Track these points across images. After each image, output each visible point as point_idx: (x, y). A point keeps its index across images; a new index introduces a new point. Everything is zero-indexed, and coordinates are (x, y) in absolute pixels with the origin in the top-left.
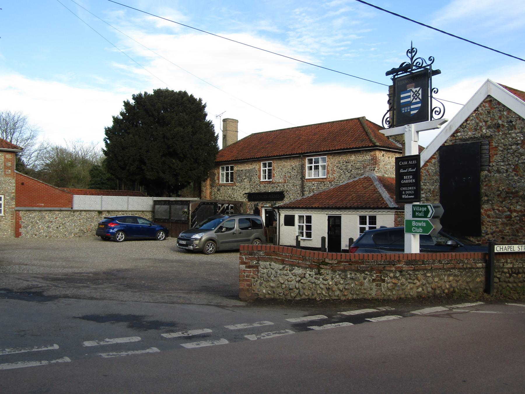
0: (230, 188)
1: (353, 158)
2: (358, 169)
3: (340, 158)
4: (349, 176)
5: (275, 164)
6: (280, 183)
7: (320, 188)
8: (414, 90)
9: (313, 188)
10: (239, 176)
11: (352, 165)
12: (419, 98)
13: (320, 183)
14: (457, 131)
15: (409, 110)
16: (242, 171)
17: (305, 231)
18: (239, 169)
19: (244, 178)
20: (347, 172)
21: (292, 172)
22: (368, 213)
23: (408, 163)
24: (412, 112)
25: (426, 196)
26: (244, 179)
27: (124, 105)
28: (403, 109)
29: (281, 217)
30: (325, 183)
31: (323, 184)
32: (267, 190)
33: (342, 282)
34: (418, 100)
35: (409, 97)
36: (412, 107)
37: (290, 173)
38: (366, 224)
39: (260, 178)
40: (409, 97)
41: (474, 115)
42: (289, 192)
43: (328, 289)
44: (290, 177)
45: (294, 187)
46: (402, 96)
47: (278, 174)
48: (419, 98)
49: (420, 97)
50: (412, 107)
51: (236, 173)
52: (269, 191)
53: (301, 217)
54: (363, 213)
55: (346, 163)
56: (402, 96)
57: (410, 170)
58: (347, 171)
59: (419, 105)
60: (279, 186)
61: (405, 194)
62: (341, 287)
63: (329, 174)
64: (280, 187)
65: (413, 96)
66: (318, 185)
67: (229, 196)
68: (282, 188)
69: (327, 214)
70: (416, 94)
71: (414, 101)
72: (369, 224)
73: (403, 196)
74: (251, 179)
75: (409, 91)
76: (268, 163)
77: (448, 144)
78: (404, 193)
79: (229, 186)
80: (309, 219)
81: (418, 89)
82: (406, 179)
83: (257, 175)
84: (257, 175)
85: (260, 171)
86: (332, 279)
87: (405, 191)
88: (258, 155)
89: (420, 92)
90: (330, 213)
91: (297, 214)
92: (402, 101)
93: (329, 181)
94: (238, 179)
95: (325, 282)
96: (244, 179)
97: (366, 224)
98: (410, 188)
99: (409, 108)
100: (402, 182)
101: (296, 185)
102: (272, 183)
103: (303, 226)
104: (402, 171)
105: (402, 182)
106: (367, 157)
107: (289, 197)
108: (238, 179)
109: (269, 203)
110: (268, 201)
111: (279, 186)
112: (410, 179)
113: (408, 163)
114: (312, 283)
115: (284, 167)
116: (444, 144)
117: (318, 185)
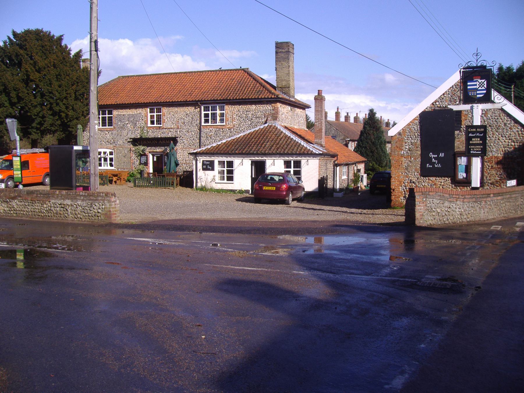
0: (109, 133)
1: (254, 107)
2: (259, 117)
3: (240, 106)
4: (250, 124)
5: (165, 110)
6: (172, 128)
7: (218, 134)
8: (480, 81)
9: (210, 134)
10: (120, 120)
11: (252, 114)
12: (484, 87)
13: (218, 129)
14: (435, 102)
15: (475, 94)
16: (123, 115)
17: (226, 175)
18: (119, 113)
19: (127, 122)
20: (247, 120)
21: (186, 119)
22: (292, 159)
23: (476, 130)
24: (478, 96)
25: (409, 148)
26: (127, 124)
27: (248, 69)
28: (470, 93)
29: (198, 162)
30: (224, 129)
31: (222, 131)
32: (157, 135)
33: (467, 209)
34: (483, 88)
35: (476, 85)
36: (478, 92)
37: (184, 119)
38: (291, 168)
39: (147, 124)
40: (476, 85)
41: (450, 90)
42: (183, 138)
43: (461, 214)
44: (184, 123)
45: (189, 133)
46: (468, 84)
47: (169, 120)
48: (484, 87)
49: (485, 86)
50: (478, 92)
51: (116, 118)
52: (159, 137)
53: (220, 162)
54: (287, 159)
55: (247, 111)
56: (468, 84)
57: (478, 134)
58: (248, 119)
59: (485, 92)
60: (170, 132)
61: (473, 150)
62: (467, 212)
63: (228, 121)
64: (172, 133)
65: (479, 85)
66: (216, 131)
67: (107, 141)
68: (174, 134)
69: (250, 159)
70: (481, 85)
71: (480, 88)
72: (294, 168)
73: (472, 152)
74: (136, 124)
75: (476, 81)
76: (204, 111)
77: (428, 110)
78: (472, 149)
79: (107, 131)
80: (230, 164)
81: (483, 81)
82: (474, 141)
83: (143, 120)
84: (143, 120)
85: (147, 116)
86: (463, 208)
87: (473, 148)
88: (142, 100)
89: (485, 83)
90: (254, 158)
91: (216, 160)
92: (469, 87)
93: (228, 128)
94: (119, 123)
95: (460, 210)
96: (127, 124)
97: (291, 168)
98: (478, 147)
99: (475, 92)
100: (471, 142)
101: (191, 131)
102: (162, 129)
103: (224, 170)
104: (470, 135)
105: (471, 142)
106: (268, 107)
107: (183, 142)
108: (119, 123)
109: (159, 148)
110: (157, 146)
111: (170, 132)
112: (478, 141)
113: (476, 130)
114: (453, 211)
115: (176, 112)
116: (425, 110)
117: (216, 131)
